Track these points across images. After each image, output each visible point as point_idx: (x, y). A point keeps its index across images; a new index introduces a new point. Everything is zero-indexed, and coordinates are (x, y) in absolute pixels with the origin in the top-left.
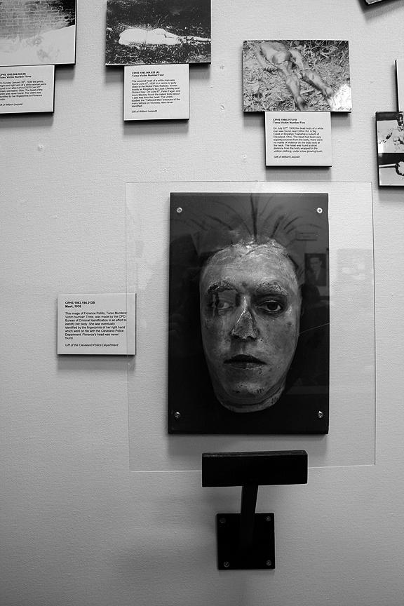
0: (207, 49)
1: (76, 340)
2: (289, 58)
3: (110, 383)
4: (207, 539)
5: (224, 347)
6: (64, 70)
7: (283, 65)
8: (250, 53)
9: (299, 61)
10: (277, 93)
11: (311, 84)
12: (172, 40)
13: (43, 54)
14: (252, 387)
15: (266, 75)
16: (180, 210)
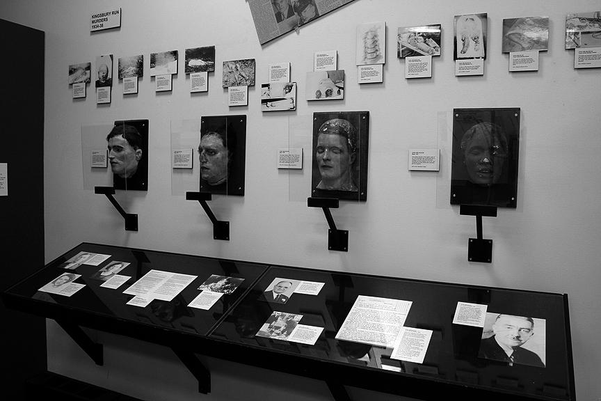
0: (213, 66)
2: (236, 67)
3: (296, 178)
4: (465, 250)
7: (234, 70)
10: (232, 80)
11: (242, 76)
13: (168, 71)
16: (457, 115)
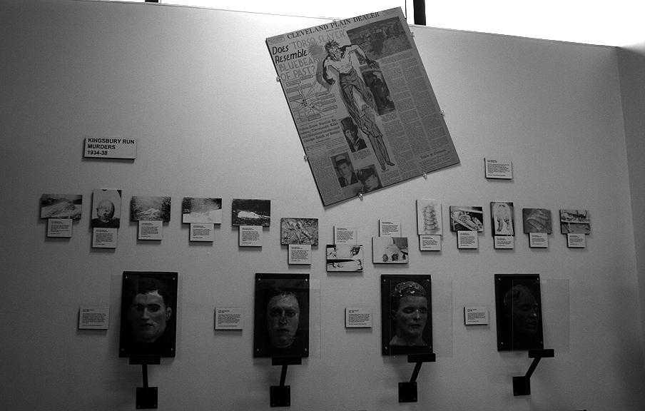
0: (269, 220)
1: (223, 324)
2: (298, 225)
5: (277, 326)
6: (217, 226)
8: (284, 223)
9: (301, 226)
10: (293, 238)
12: (257, 217)
14: (285, 338)
15: (289, 231)
